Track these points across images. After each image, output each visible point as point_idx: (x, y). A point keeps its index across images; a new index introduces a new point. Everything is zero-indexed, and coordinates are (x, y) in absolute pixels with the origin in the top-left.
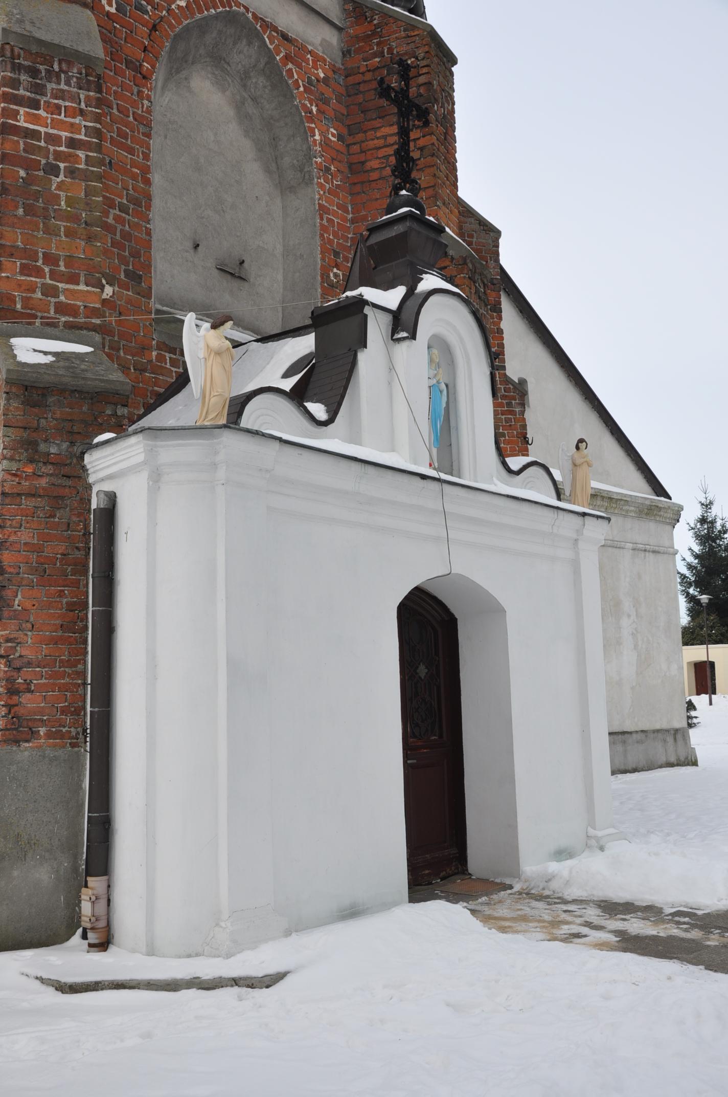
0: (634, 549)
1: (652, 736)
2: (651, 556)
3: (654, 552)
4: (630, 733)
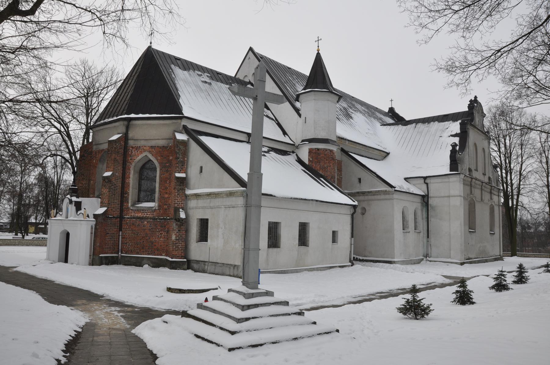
0: (225, 207)
1: (225, 265)
2: (232, 209)
3: (233, 207)
4: (218, 263)
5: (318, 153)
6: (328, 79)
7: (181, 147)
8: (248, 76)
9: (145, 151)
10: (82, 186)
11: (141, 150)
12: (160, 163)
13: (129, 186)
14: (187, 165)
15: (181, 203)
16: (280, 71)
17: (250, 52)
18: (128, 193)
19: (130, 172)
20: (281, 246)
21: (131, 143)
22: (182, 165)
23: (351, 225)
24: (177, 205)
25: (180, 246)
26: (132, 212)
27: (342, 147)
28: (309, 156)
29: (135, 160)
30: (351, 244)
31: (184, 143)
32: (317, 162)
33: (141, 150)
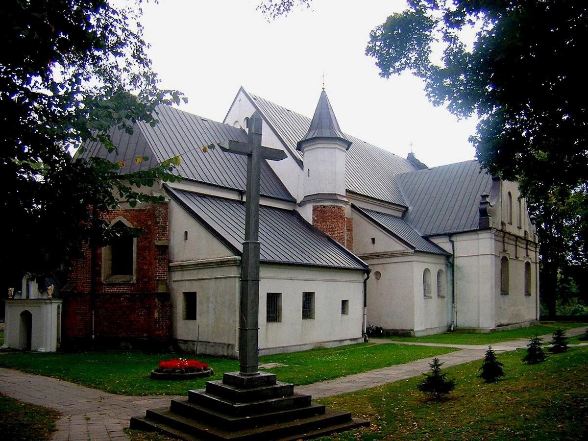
7: (161, 210)
9: (118, 215)
13: (101, 257)
17: (241, 92)
18: (100, 266)
22: (163, 231)
23: (364, 293)
26: (106, 287)
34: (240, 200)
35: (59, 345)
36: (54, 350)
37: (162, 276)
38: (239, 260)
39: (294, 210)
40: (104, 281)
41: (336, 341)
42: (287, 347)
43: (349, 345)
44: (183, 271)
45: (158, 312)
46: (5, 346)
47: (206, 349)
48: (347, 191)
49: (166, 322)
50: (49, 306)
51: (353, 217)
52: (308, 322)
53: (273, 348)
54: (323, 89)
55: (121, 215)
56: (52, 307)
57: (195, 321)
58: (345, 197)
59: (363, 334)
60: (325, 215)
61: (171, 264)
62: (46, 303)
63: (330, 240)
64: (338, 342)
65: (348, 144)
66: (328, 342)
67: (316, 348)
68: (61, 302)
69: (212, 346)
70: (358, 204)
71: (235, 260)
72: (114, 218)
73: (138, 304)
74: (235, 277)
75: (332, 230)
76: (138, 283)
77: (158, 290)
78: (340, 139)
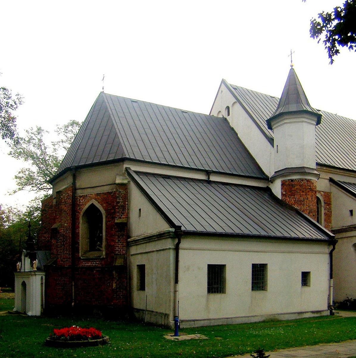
5: (292, 185)
6: (304, 96)
7: (120, 191)
8: (221, 111)
9: (91, 198)
10: (45, 239)
11: (88, 198)
12: (106, 210)
13: (79, 236)
14: (128, 209)
15: (123, 250)
16: (341, 125)
17: (223, 84)
18: (78, 243)
19: (79, 222)
20: (227, 292)
21: (79, 193)
22: (123, 210)
23: (329, 264)
24: (118, 252)
25: (121, 294)
26: (83, 262)
27: (330, 177)
28: (281, 189)
29: (82, 209)
30: (330, 287)
31: (124, 186)
32: (292, 195)
33: (88, 198)
34: (207, 179)
35: (43, 310)
36: (38, 313)
37: (121, 250)
38: (172, 232)
39: (267, 187)
40: (82, 255)
41: (295, 313)
42: (231, 318)
43: (310, 318)
44: (137, 245)
45: (115, 283)
46: (15, 310)
47: (151, 318)
48: (318, 164)
49: (123, 292)
50: (34, 277)
51: (332, 191)
52: (259, 294)
53: (214, 319)
54: (292, 66)
55: (93, 198)
56: (36, 278)
57: (144, 291)
58: (315, 170)
59: (329, 306)
60: (293, 189)
61: (129, 240)
62: (32, 275)
63: (298, 213)
64: (297, 314)
65: (318, 117)
66: (285, 314)
67: (267, 320)
68: (45, 274)
69: (155, 315)
70: (336, 178)
71: (169, 232)
72: (88, 201)
73: (107, 276)
74: (170, 249)
75: (300, 203)
76: (106, 258)
77: (115, 263)
78: (307, 112)
